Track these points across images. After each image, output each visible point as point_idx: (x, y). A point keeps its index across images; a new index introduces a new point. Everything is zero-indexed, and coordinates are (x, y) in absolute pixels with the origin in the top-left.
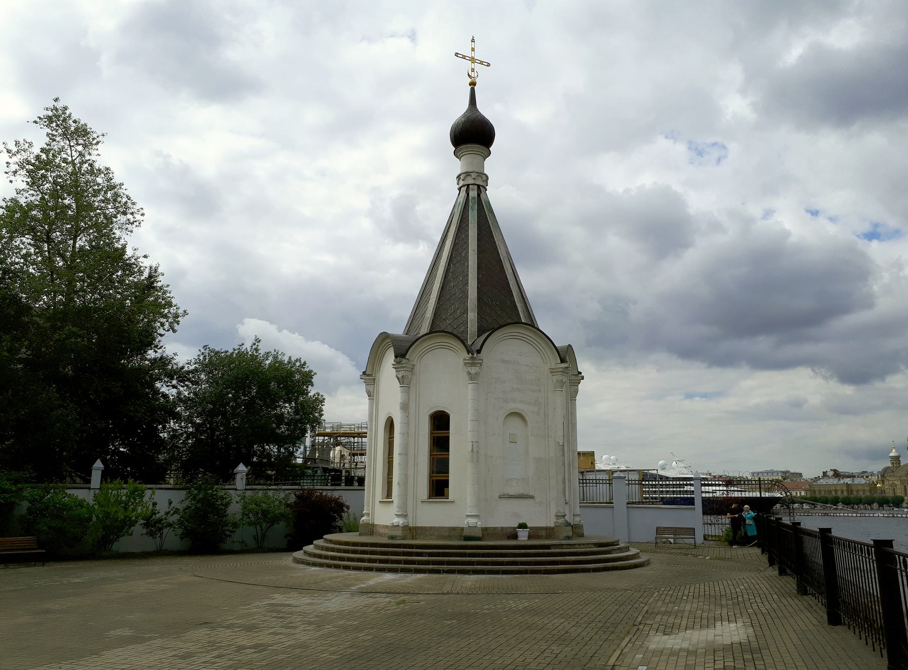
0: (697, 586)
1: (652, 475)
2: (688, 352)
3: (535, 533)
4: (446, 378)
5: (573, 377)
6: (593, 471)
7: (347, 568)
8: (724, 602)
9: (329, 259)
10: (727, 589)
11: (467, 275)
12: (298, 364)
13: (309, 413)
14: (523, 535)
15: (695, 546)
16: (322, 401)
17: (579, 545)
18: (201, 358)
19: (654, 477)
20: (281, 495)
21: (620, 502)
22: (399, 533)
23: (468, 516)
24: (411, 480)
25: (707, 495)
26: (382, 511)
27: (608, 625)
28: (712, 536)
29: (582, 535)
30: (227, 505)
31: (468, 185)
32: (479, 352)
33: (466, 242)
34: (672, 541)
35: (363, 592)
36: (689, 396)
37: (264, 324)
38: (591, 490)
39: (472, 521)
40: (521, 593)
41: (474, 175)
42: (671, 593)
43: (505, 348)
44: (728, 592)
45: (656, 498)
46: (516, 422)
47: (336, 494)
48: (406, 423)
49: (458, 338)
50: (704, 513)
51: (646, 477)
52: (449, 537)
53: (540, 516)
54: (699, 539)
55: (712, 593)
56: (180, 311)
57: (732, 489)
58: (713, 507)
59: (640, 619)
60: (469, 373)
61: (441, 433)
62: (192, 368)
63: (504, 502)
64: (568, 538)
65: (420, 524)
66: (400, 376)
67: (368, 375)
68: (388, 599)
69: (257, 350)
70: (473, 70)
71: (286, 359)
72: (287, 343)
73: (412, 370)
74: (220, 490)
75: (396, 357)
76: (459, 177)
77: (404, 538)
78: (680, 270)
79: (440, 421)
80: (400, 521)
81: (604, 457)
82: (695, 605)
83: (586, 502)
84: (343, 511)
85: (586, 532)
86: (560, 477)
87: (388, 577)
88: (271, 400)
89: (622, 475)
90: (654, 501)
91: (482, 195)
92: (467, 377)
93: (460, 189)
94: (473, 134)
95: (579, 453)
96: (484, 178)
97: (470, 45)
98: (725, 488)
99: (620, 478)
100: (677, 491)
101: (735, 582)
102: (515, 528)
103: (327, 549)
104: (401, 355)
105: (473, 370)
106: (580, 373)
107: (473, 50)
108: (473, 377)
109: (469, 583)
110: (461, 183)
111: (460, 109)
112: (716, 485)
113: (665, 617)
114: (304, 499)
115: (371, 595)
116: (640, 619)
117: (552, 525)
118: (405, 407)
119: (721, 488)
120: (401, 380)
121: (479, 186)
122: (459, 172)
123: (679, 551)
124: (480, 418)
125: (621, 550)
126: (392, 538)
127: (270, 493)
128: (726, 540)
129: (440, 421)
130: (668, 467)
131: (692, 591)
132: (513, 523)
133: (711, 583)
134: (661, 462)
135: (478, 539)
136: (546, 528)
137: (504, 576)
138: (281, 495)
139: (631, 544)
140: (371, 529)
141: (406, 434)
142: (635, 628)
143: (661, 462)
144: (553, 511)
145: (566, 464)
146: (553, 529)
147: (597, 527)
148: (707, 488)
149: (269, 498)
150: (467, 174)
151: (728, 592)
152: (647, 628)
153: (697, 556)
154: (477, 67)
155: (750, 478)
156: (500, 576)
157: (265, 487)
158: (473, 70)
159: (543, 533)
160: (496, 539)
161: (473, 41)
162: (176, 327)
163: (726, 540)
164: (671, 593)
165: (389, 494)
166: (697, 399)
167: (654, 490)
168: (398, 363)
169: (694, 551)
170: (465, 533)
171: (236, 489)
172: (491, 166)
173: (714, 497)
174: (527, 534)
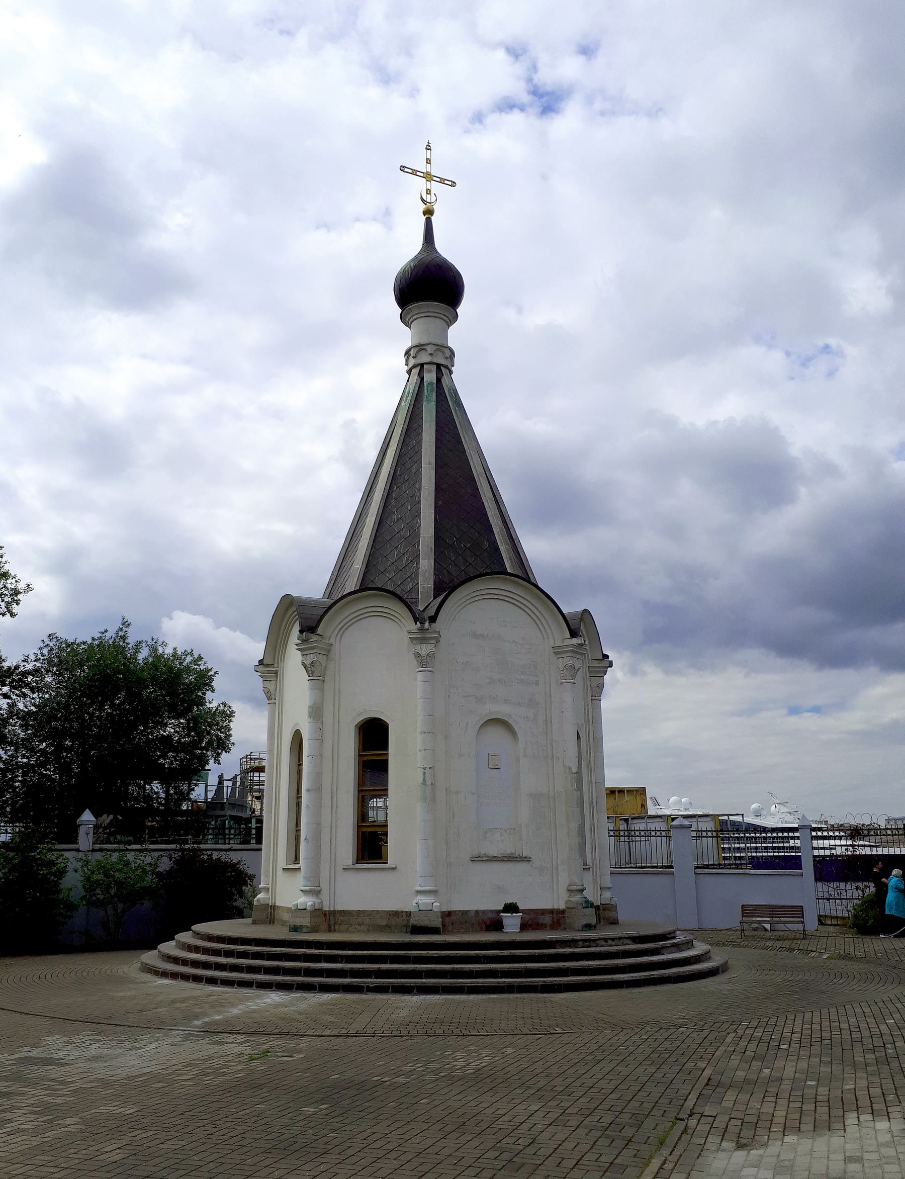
0: (808, 1015)
1: (734, 823)
2: (791, 646)
3: (532, 920)
4: (381, 666)
5: (595, 664)
6: (643, 816)
7: (212, 981)
8: (859, 1058)
9: (287, 529)
10: (863, 1026)
11: (419, 502)
12: (189, 659)
13: (210, 734)
14: (512, 923)
15: (805, 935)
16: (231, 714)
17: (606, 940)
18: (45, 651)
19: (737, 827)
20: (153, 858)
21: (685, 865)
22: (305, 921)
23: (419, 892)
24: (326, 837)
25: (822, 853)
26: (285, 887)
27: (625, 1118)
28: (832, 917)
29: (614, 922)
30: (62, 873)
31: (422, 365)
32: (433, 619)
33: (419, 452)
34: (768, 926)
35: (209, 1031)
36: (794, 711)
37: (197, 619)
38: (639, 846)
39: (425, 901)
40: (497, 1027)
41: (430, 349)
42: (758, 1034)
43: (479, 616)
44: (866, 1033)
45: (741, 858)
46: (497, 735)
47: (234, 857)
48: (320, 740)
49: (401, 599)
50: (817, 879)
51: (727, 829)
52: (387, 928)
53: (542, 892)
54: (811, 923)
55: (836, 1034)
56: (21, 586)
57: (861, 843)
58: (830, 870)
59: (690, 1104)
60: (418, 655)
61: (373, 755)
62: (30, 667)
63: (479, 866)
64: (588, 927)
65: (343, 905)
66: (308, 663)
67: (268, 665)
68: (242, 1048)
69: (124, 638)
70: (429, 192)
71: (169, 651)
72: (179, 632)
73: (327, 651)
74: (48, 851)
75: (301, 631)
76: (407, 353)
77: (314, 929)
78: (778, 531)
79: (373, 734)
80: (307, 901)
81: (672, 799)
82: (803, 1065)
83: (627, 867)
84: (246, 884)
85: (622, 917)
86: (574, 825)
87: (274, 997)
88: (150, 713)
89: (686, 822)
90: (738, 863)
91: (445, 381)
92: (415, 662)
93: (409, 372)
94: (430, 287)
95: (612, 792)
96: (448, 354)
97: (423, 154)
98: (849, 842)
99: (682, 827)
100: (778, 848)
101: (875, 1009)
102: (499, 912)
103: (197, 949)
104: (309, 628)
105: (424, 650)
106: (606, 657)
107: (428, 161)
108: (423, 662)
109: (404, 1013)
110: (412, 362)
111: (410, 248)
112: (835, 838)
113: (744, 1097)
114: (188, 864)
115: (218, 1038)
116: (690, 1104)
117: (562, 906)
118: (316, 713)
119: (844, 842)
120: (310, 669)
121: (439, 366)
122: (408, 344)
123: (779, 944)
124: (437, 728)
125: (677, 947)
126: (295, 929)
127: (130, 856)
128: (854, 925)
129: (373, 734)
130: (764, 812)
131: (798, 1029)
132: (489, 902)
133: (833, 1011)
134: (753, 806)
135: (434, 931)
136: (551, 912)
137: (472, 997)
138: (153, 858)
139: (701, 932)
140: (270, 914)
141: (319, 756)
142: (681, 1126)
143: (753, 806)
144: (564, 879)
145: (586, 805)
146: (563, 912)
147: (643, 908)
148: (821, 843)
149: (127, 864)
150: (421, 347)
151: (866, 1033)
152: (703, 1128)
153: (807, 952)
154: (435, 186)
155: (883, 827)
156: (464, 997)
157: (122, 847)
158: (429, 192)
159: (547, 919)
160: (467, 931)
161: (428, 148)
162: (15, 608)
163: (854, 925)
164: (758, 1034)
165: (296, 860)
166: (806, 714)
167: (744, 848)
168: (304, 641)
169: (803, 944)
170: (413, 921)
171: (78, 850)
172: (456, 336)
173: (831, 856)
174: (518, 922)
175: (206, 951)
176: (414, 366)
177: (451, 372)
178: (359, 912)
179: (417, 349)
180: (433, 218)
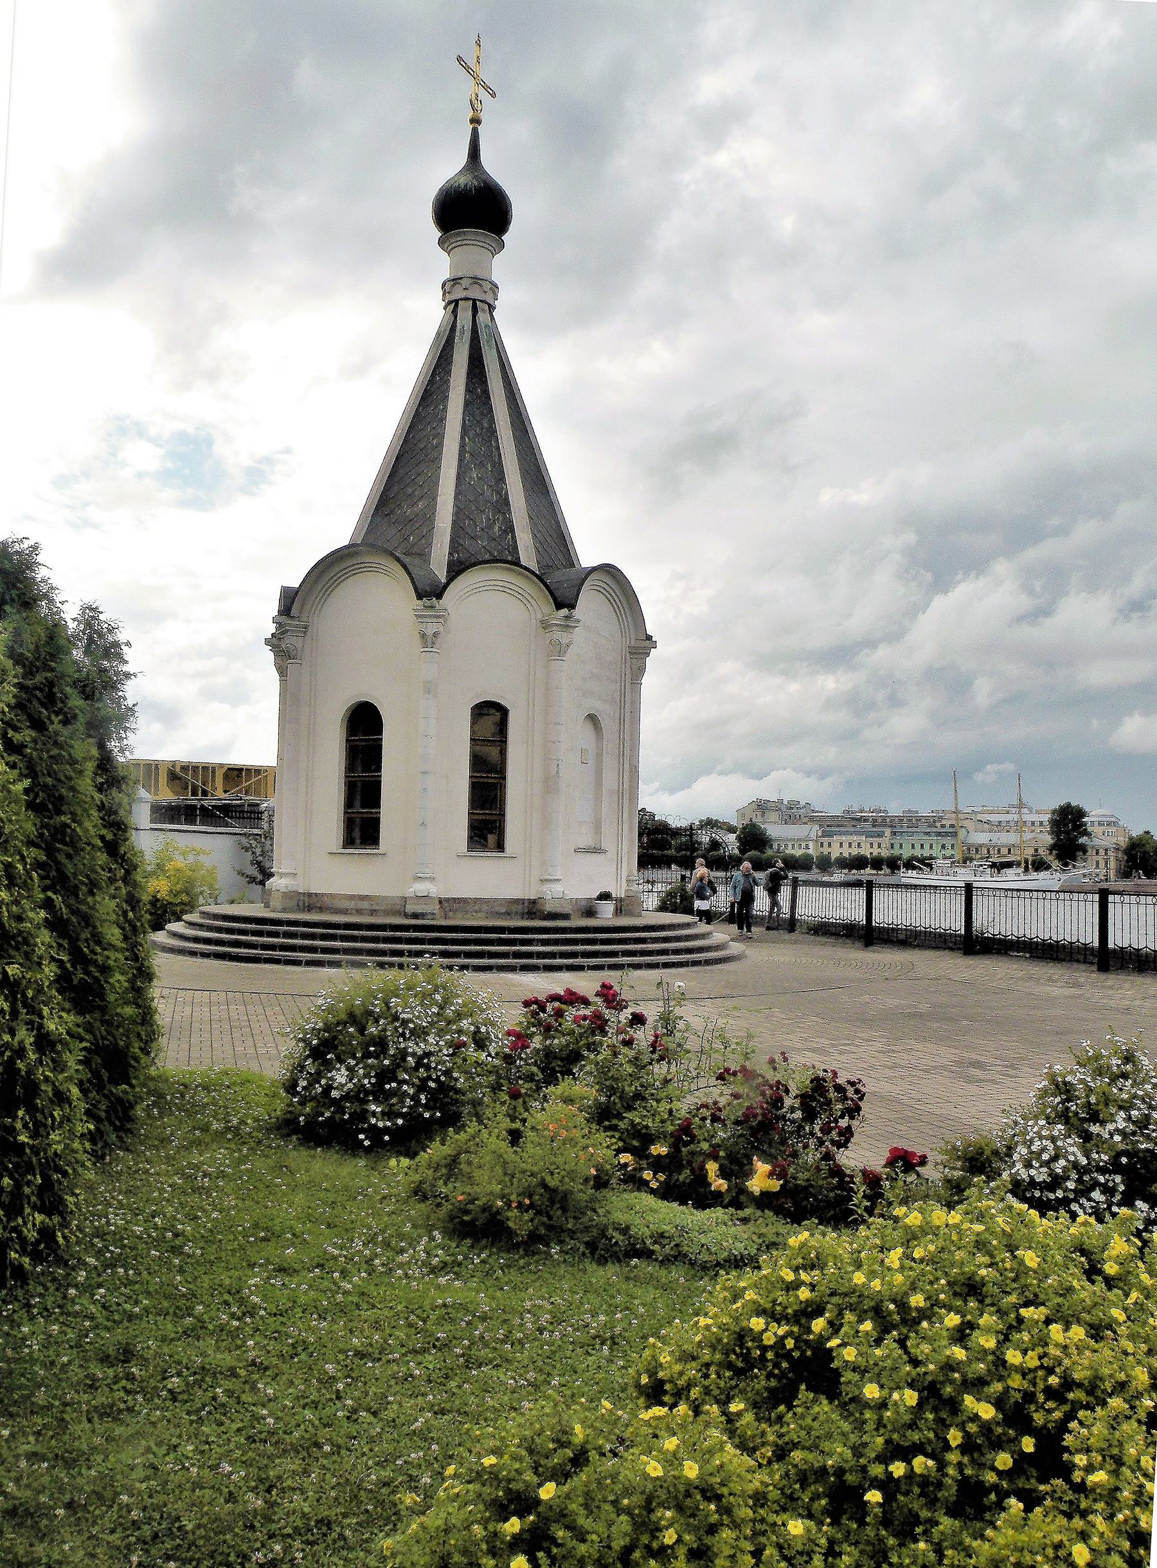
79: (491, 718)
93: (445, 308)
103: (201, 926)
111: (447, 168)
122: (447, 275)
129: (491, 718)
150: (455, 281)
175: (219, 930)
176: (450, 303)
177: (491, 308)
178: (476, 900)
179: (471, 281)
180: (481, 129)
